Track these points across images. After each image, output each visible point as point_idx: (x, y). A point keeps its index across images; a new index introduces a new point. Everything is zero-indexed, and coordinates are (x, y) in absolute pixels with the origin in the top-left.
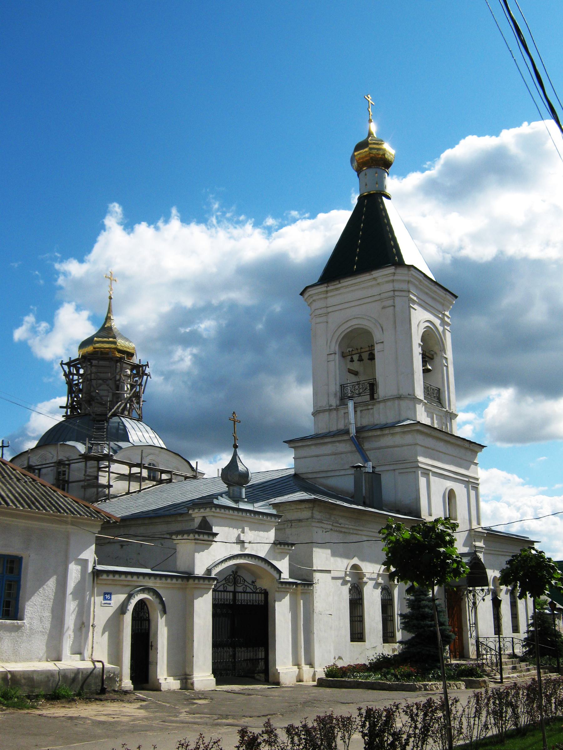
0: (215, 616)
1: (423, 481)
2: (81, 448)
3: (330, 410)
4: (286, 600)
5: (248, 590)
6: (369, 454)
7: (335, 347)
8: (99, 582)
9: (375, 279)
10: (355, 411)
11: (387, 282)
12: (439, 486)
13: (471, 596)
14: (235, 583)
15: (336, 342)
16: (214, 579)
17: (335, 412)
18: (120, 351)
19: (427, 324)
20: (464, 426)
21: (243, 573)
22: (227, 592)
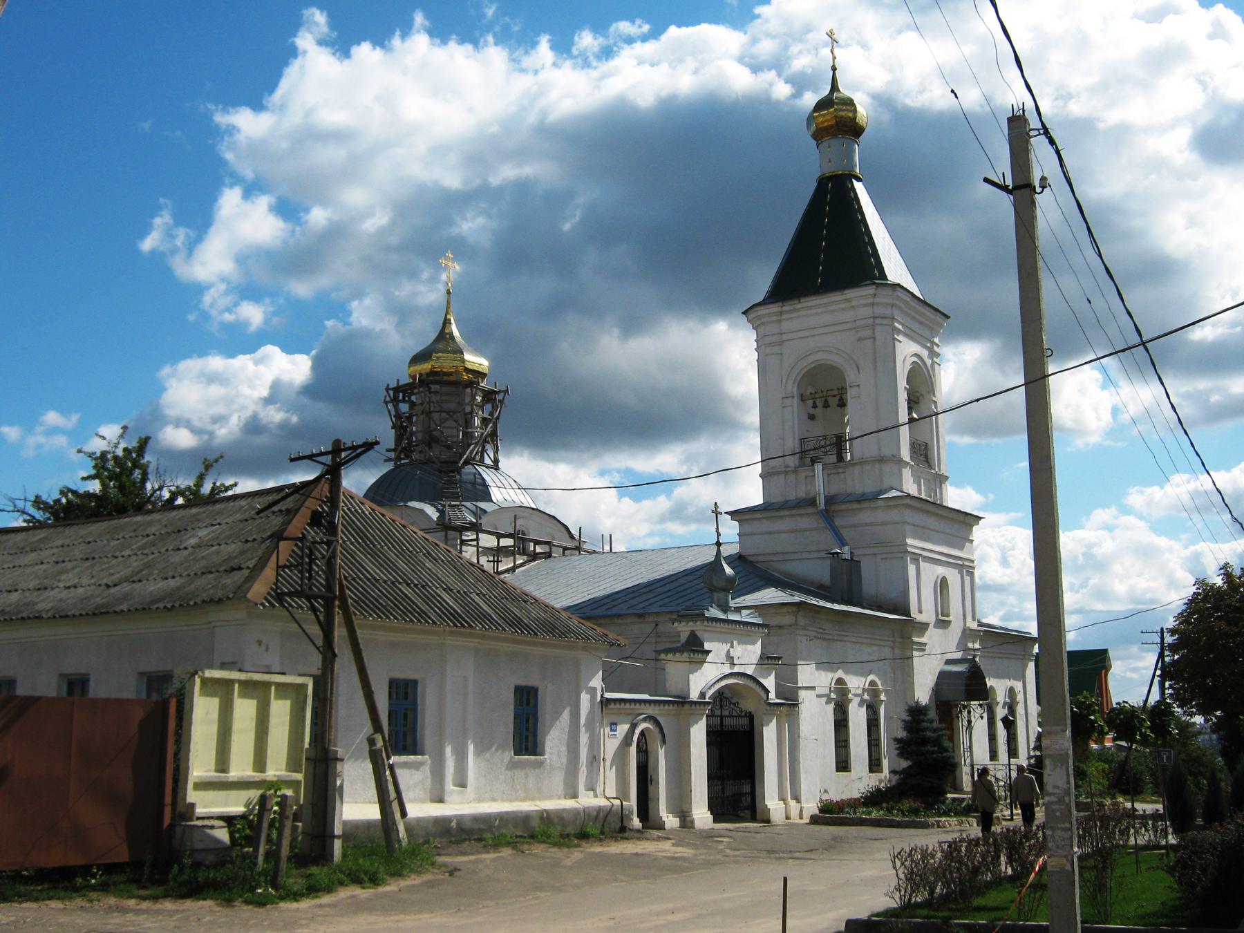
0: (709, 744)
1: (912, 569)
2: (432, 512)
3: (786, 472)
4: (774, 724)
6: (846, 533)
7: (793, 389)
9: (848, 300)
11: (866, 305)
12: (930, 573)
13: (965, 713)
16: (708, 703)
17: (792, 476)
18: (467, 370)
20: (956, 497)
21: (728, 694)
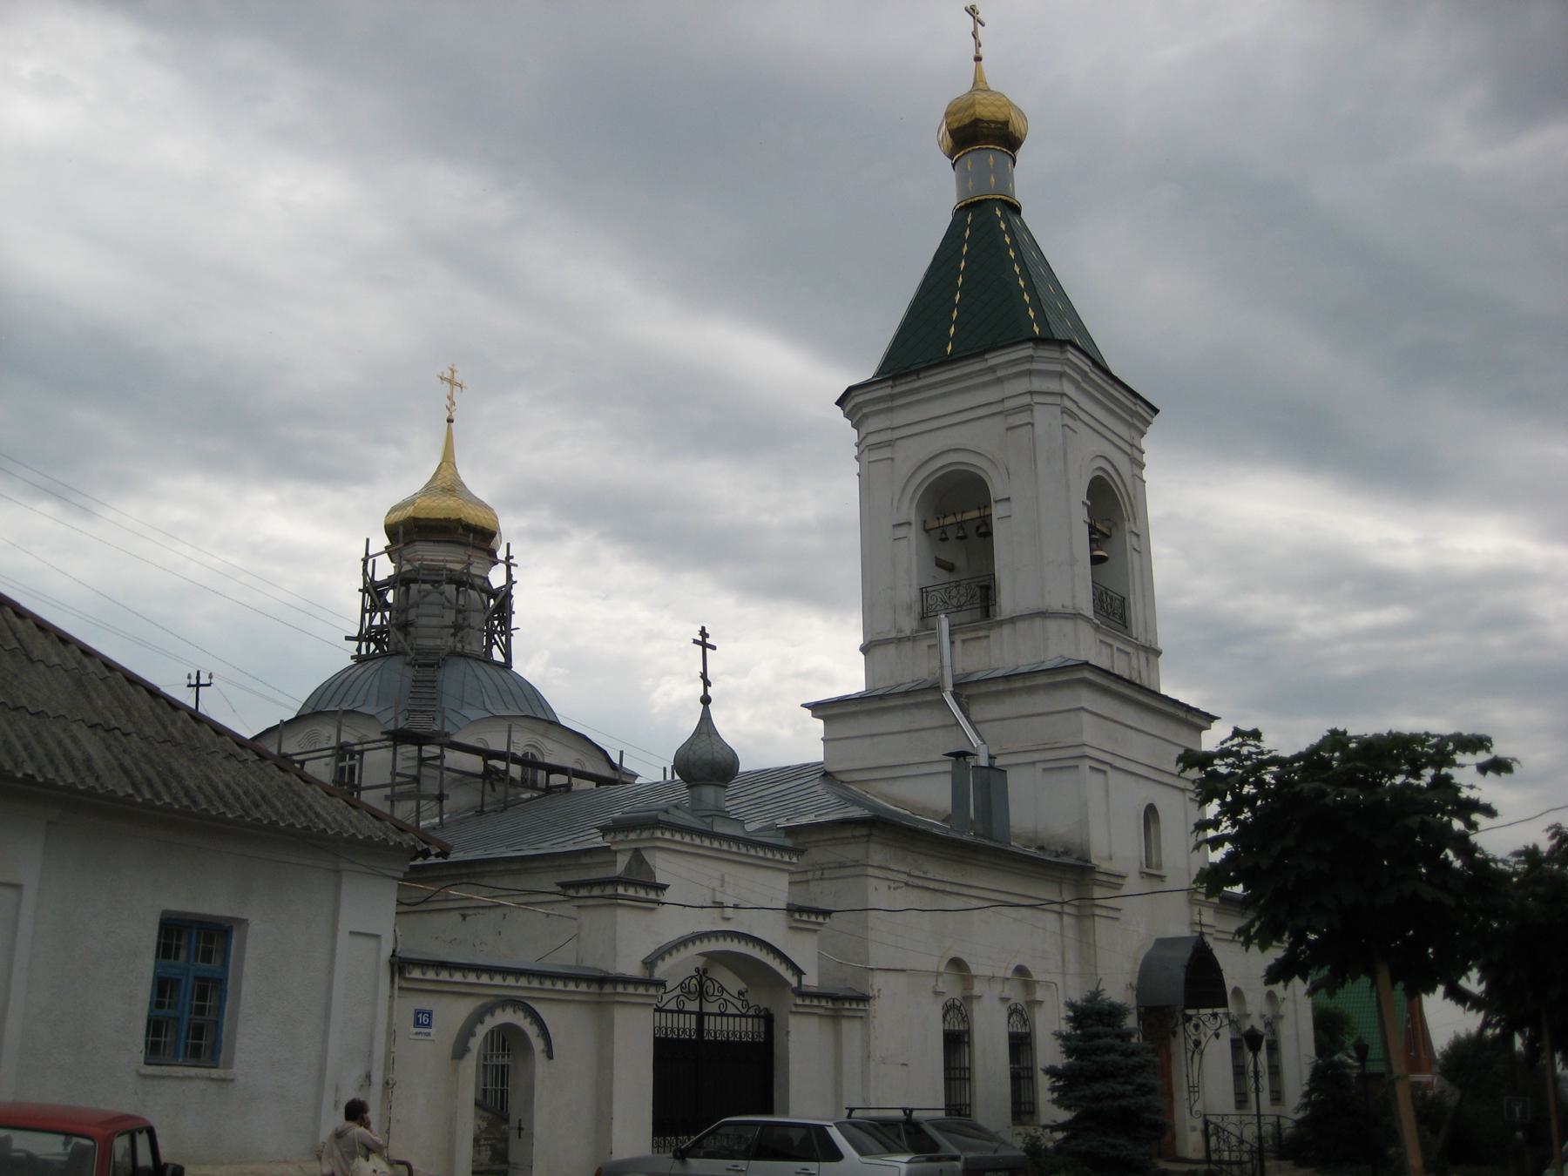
3: (899, 640)
5: (731, 1010)
7: (909, 512)
8: (405, 985)
10: (952, 643)
14: (702, 994)
15: (913, 498)
19: (1102, 463)
22: (685, 1013)
